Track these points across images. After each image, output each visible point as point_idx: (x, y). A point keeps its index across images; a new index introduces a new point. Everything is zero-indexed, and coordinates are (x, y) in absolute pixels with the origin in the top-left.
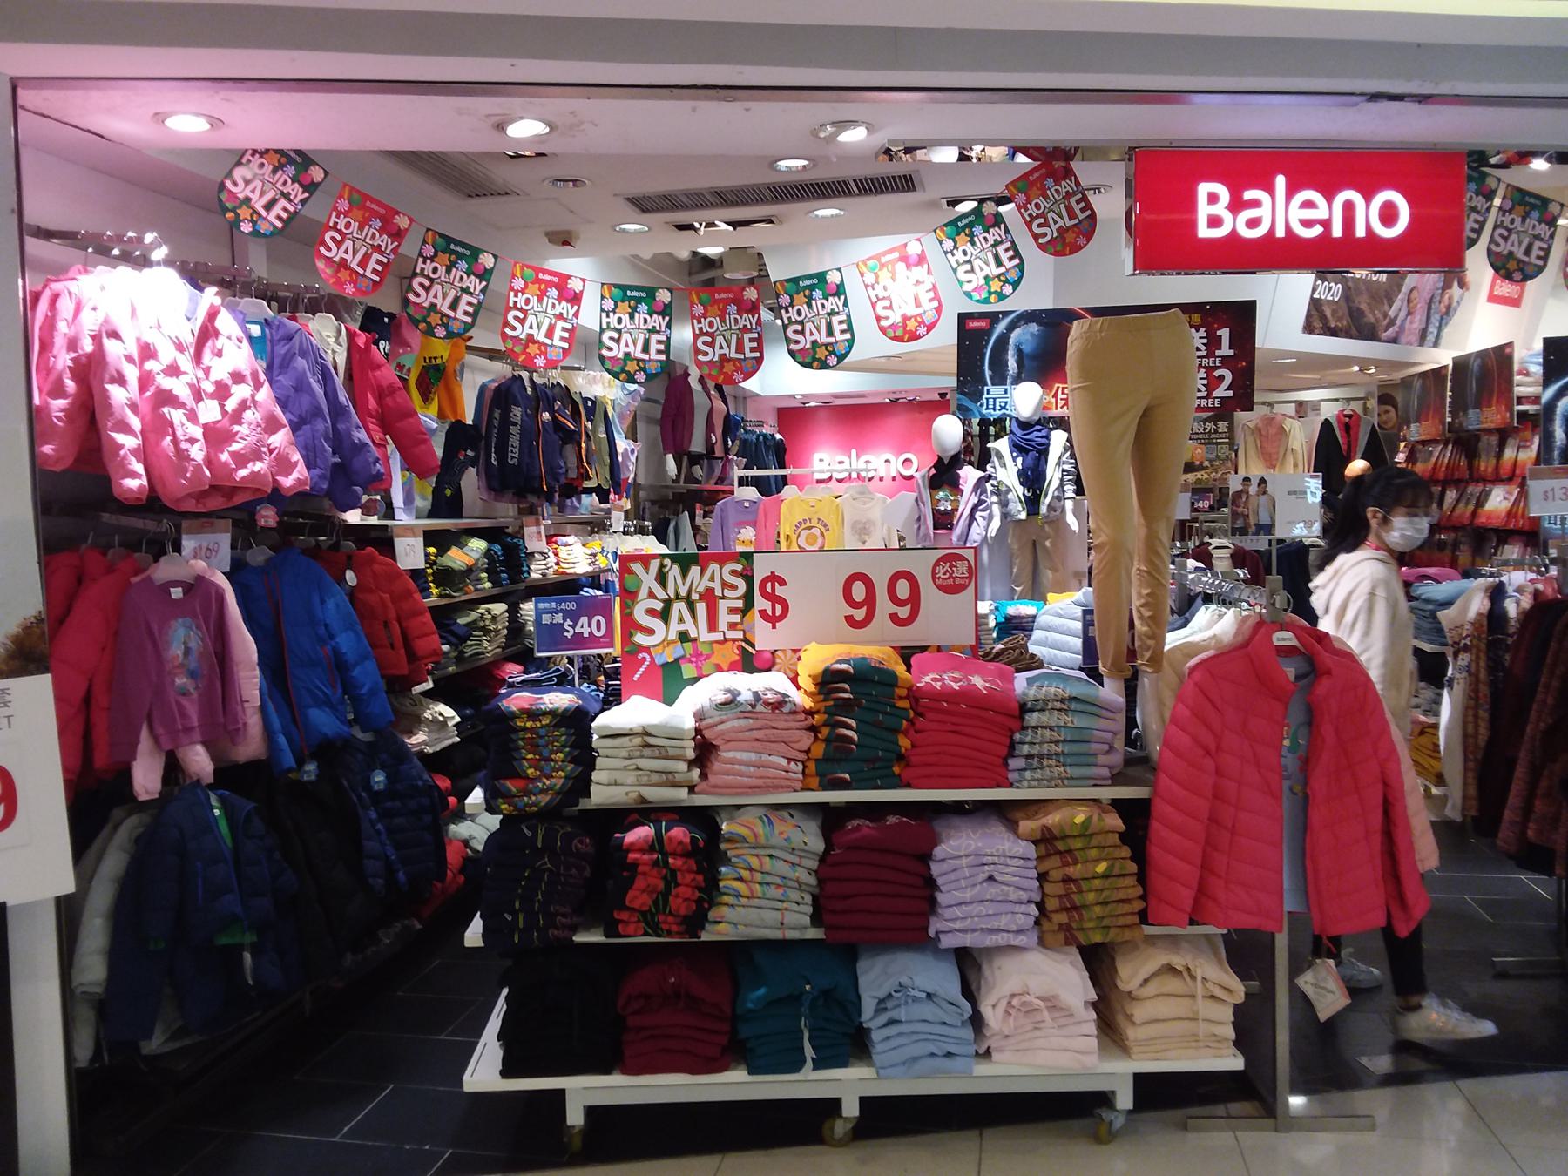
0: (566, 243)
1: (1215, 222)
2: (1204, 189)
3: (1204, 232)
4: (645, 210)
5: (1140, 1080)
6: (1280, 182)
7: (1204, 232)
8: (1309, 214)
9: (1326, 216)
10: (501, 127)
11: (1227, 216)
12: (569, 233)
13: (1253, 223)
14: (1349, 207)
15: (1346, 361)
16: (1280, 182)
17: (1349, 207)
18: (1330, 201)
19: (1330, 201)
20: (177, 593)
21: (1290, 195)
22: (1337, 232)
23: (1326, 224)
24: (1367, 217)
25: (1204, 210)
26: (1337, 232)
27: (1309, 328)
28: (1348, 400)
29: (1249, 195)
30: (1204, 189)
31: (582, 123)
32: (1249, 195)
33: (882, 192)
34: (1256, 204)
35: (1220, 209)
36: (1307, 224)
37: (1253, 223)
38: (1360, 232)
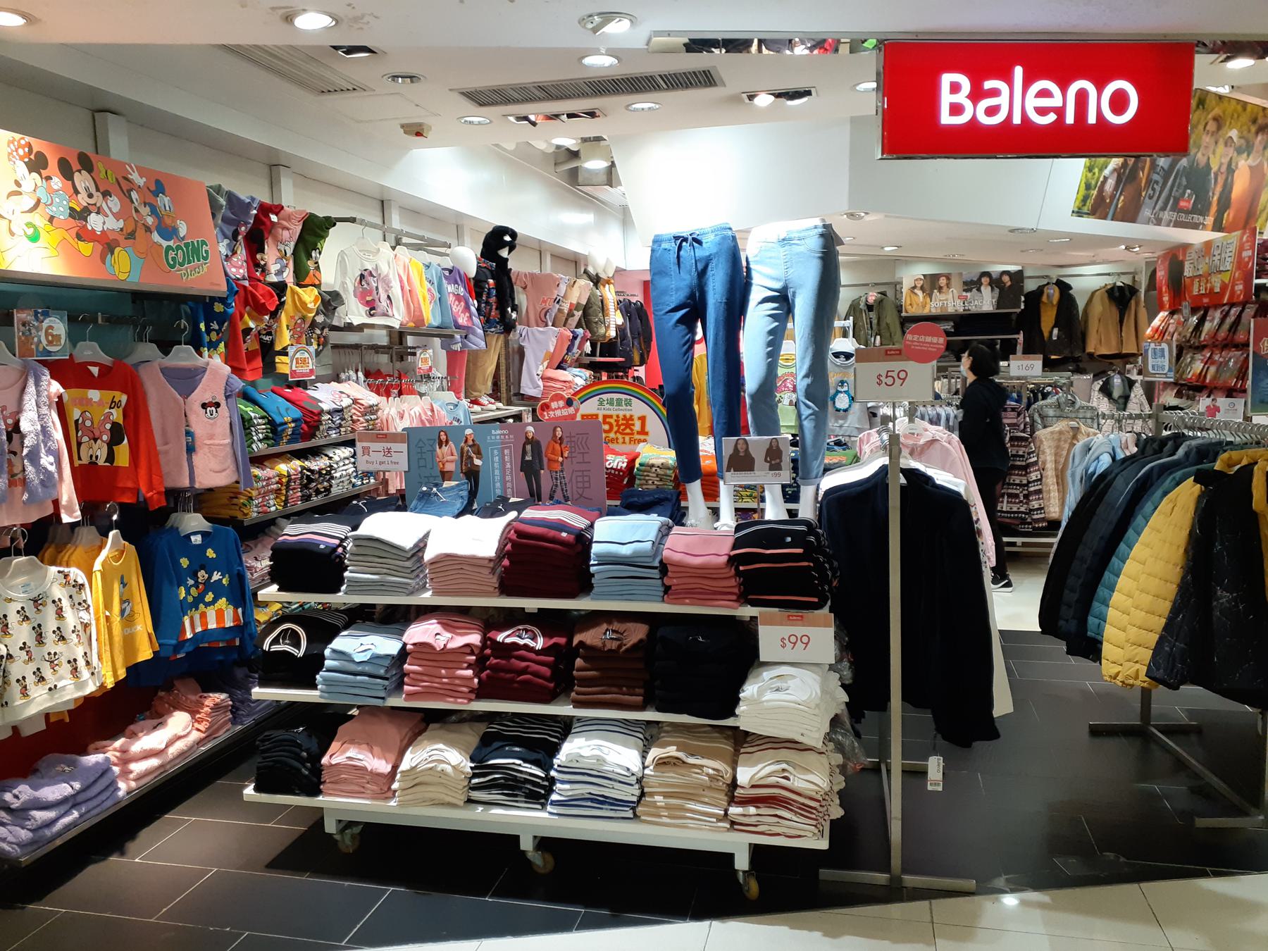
0: (418, 134)
1: (956, 109)
2: (947, 79)
3: (946, 119)
4: (482, 104)
6: (1018, 71)
7: (946, 119)
8: (1044, 102)
9: (1060, 104)
10: (289, 19)
11: (968, 105)
12: (420, 125)
13: (991, 111)
14: (1082, 97)
15: (1112, 241)
16: (1018, 71)
17: (1082, 97)
18: (1064, 91)
19: (1064, 91)
20: (95, 370)
21: (1027, 83)
22: (1070, 119)
23: (1060, 112)
24: (1099, 105)
25: (946, 98)
26: (1070, 119)
27: (1079, 213)
28: (1119, 274)
29: (988, 85)
30: (947, 79)
31: (363, 16)
32: (988, 85)
33: (687, 87)
34: (995, 93)
35: (962, 98)
36: (1042, 111)
37: (991, 111)
38: (1092, 119)
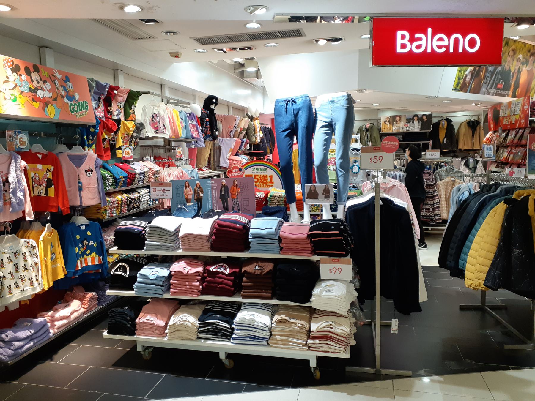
0: (177, 57)
1: (403, 46)
2: (400, 33)
3: (399, 50)
4: (203, 44)
5: (320, 359)
6: (430, 30)
7: (399, 50)
8: (441, 43)
9: (447, 44)
10: (122, 8)
11: (408, 44)
12: (177, 53)
13: (418, 47)
14: (456, 41)
15: (469, 102)
16: (430, 30)
17: (456, 41)
18: (449, 38)
19: (449, 38)
21: (433, 35)
22: (451, 50)
23: (447, 47)
24: (464, 44)
25: (399, 41)
26: (451, 50)
27: (455, 90)
28: (472, 116)
29: (417, 36)
30: (400, 33)
31: (153, 7)
32: (417, 36)
33: (290, 37)
34: (420, 39)
35: (406, 41)
36: (440, 47)
37: (418, 47)
38: (461, 50)
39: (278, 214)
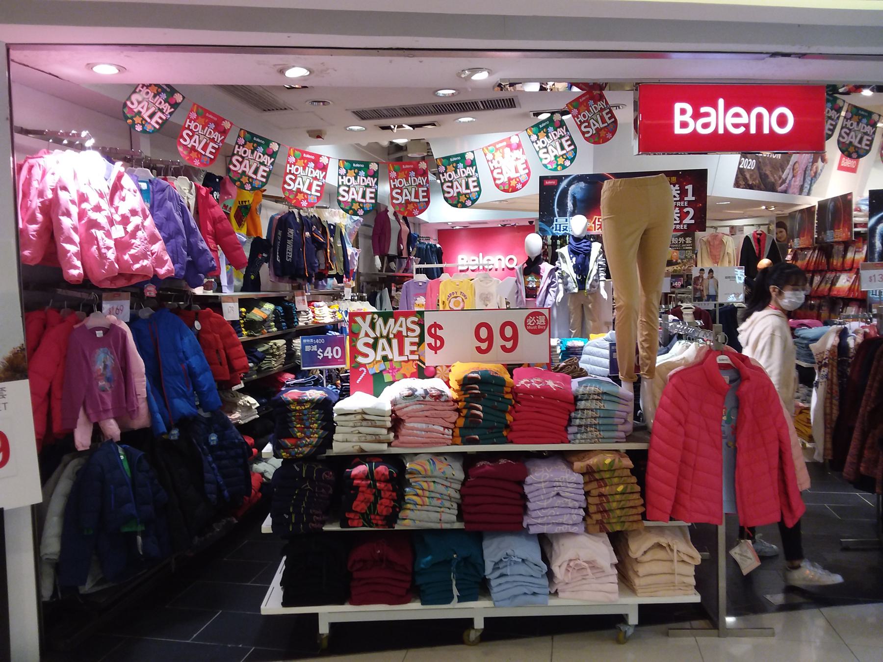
0: (319, 137)
1: (684, 125)
2: (678, 106)
3: (678, 130)
4: (363, 118)
6: (721, 102)
7: (678, 130)
8: (737, 120)
9: (747, 122)
10: (282, 71)
11: (691, 122)
12: (320, 131)
13: (706, 126)
14: (759, 116)
15: (758, 203)
16: (721, 102)
17: (759, 116)
18: (749, 113)
19: (749, 113)
21: (726, 110)
22: (753, 130)
23: (747, 126)
24: (770, 122)
25: (678, 118)
26: (753, 130)
27: (737, 185)
28: (759, 225)
29: (703, 110)
30: (678, 106)
31: (328, 69)
32: (703, 110)
33: (497, 108)
34: (707, 115)
35: (687, 118)
36: (736, 126)
37: (706, 126)
38: (766, 131)
39: (548, 556)
